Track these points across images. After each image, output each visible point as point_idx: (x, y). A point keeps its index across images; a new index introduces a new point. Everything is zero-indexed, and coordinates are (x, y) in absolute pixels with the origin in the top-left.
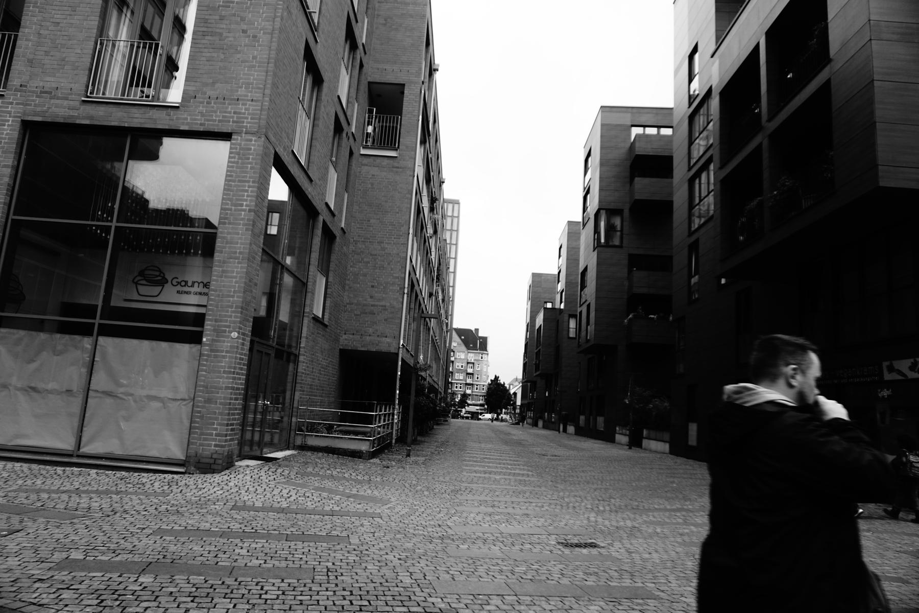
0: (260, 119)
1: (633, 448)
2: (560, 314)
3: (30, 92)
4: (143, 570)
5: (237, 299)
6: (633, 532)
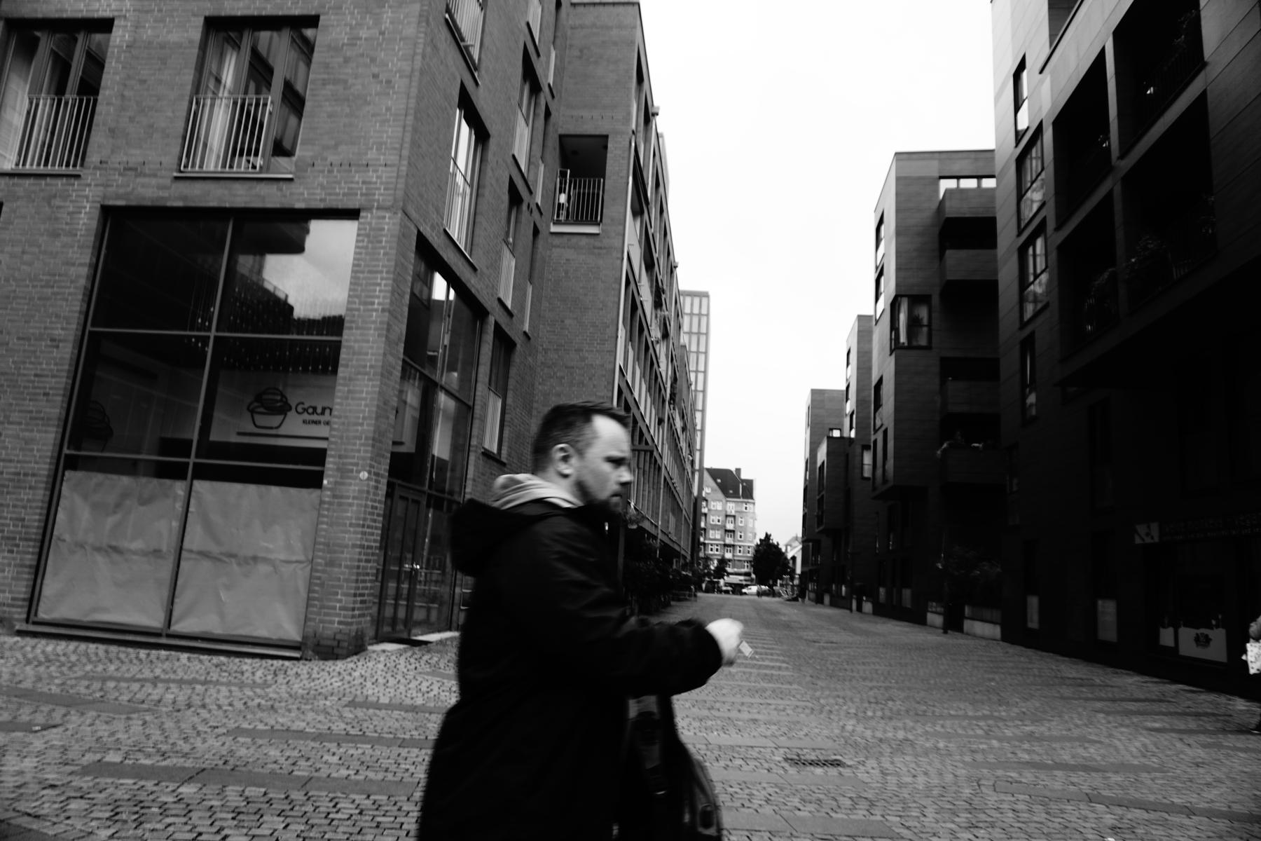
0: (395, 189)
1: (949, 631)
2: (850, 445)
3: (111, 169)
4: (191, 778)
5: (367, 428)
6: (900, 747)
